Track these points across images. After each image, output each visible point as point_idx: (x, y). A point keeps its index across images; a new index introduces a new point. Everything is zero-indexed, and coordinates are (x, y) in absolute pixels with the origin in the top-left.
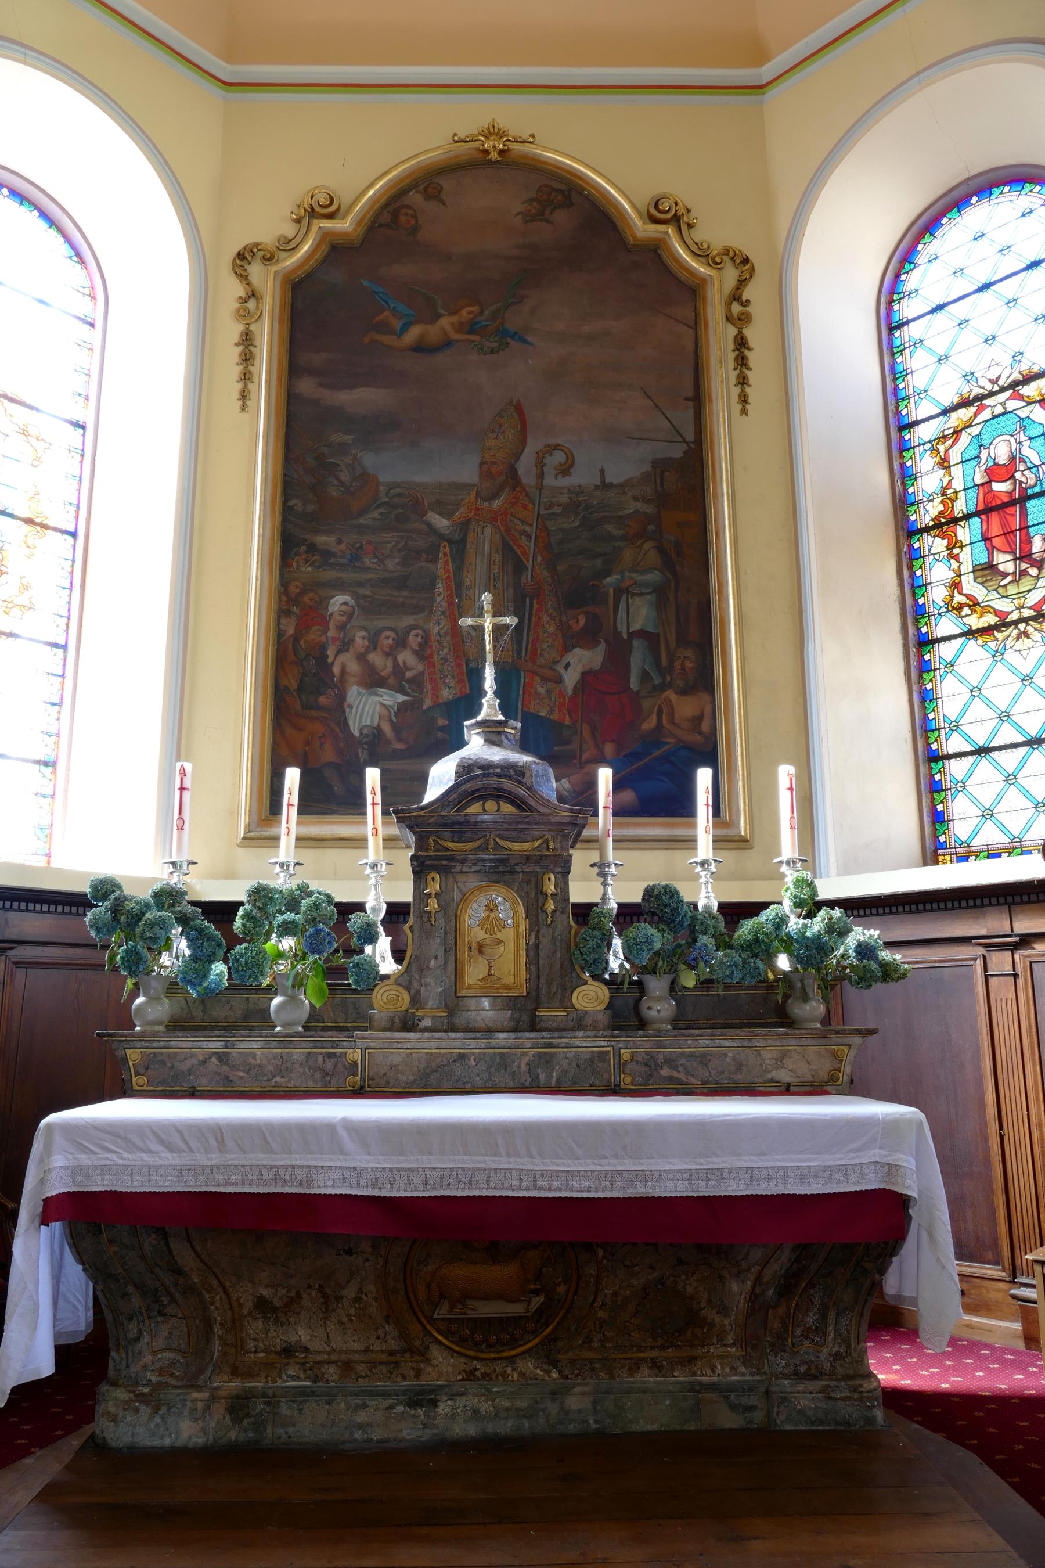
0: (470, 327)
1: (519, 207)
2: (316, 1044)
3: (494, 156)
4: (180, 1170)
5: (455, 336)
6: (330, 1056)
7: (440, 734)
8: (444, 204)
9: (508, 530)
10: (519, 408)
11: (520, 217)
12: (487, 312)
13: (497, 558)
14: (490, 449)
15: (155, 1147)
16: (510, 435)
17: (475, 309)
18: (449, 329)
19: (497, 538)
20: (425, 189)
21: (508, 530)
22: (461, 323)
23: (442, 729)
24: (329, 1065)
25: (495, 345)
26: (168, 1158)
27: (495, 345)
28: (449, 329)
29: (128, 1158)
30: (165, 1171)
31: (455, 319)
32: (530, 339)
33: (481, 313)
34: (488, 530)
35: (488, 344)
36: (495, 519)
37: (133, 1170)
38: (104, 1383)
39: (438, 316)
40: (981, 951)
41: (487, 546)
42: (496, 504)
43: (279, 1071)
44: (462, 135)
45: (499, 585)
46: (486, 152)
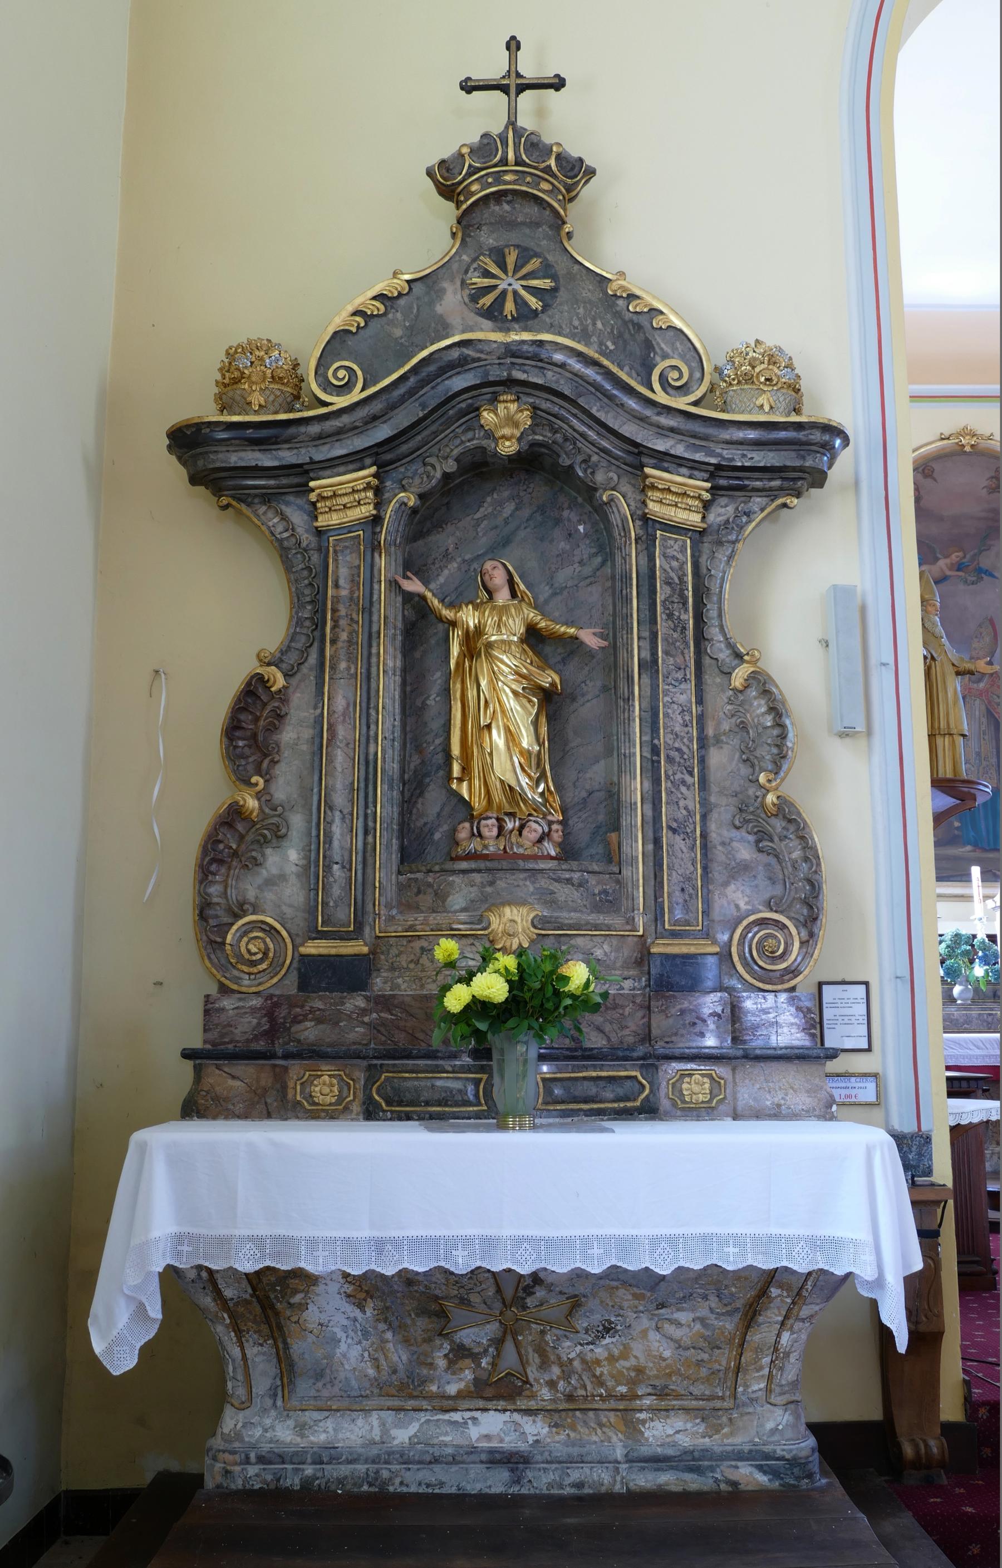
0: (960, 567)
1: (986, 483)
2: (983, 1009)
3: (968, 449)
4: (984, 1056)
5: (948, 573)
6: (990, 1015)
7: (956, 832)
8: (935, 480)
9: (990, 702)
10: (992, 622)
11: (985, 490)
12: (968, 556)
13: (984, 720)
14: (975, 649)
15: (972, 1047)
16: (987, 639)
17: (961, 554)
18: (945, 568)
19: (983, 707)
20: (923, 470)
21: (990, 702)
22: (952, 564)
23: (957, 828)
24: (990, 1019)
25: (974, 579)
26: (978, 1052)
27: (974, 579)
28: (945, 568)
29: (962, 1052)
30: (977, 1057)
31: (948, 561)
32: (996, 574)
33: (964, 557)
34: (978, 702)
35: (970, 578)
36: (981, 695)
37: (964, 1057)
38: (229, 1412)
39: (937, 559)
40: (262, 517)
41: (977, 713)
42: (982, 685)
43: (966, 1022)
44: (947, 434)
45: (986, 737)
46: (963, 446)
